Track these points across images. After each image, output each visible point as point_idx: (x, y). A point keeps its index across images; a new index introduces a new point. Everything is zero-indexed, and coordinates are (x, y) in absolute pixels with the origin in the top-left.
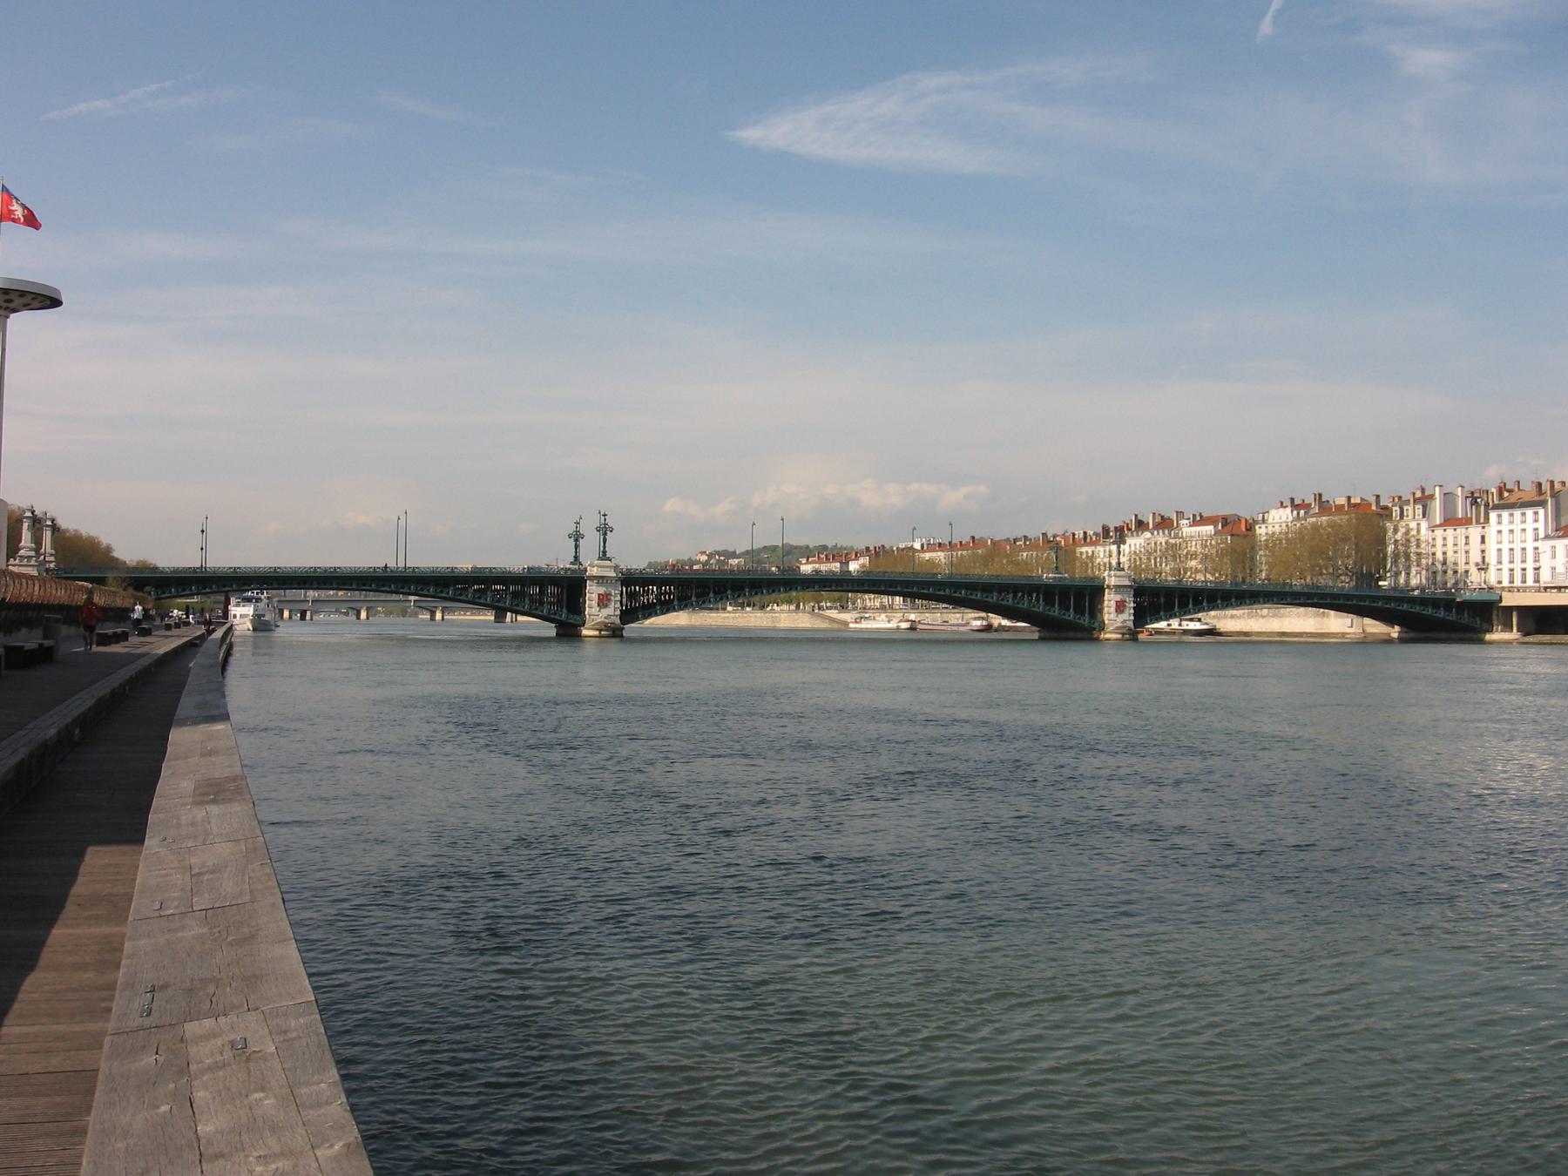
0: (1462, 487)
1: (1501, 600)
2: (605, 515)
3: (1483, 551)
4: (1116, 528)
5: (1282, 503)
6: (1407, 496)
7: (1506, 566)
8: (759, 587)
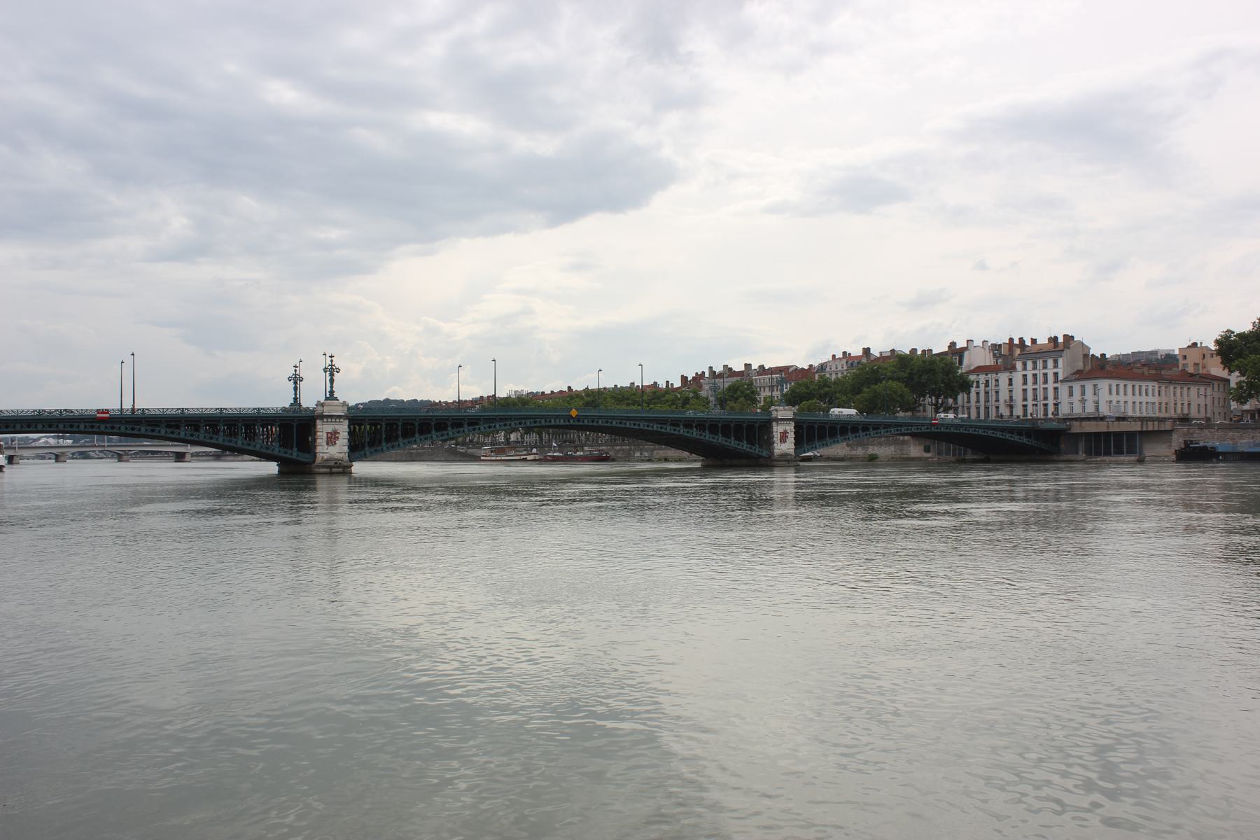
1: (1070, 429)
2: (331, 357)
3: (1011, 391)
4: (316, 405)
6: (322, 400)
7: (1041, 403)
8: (476, 424)
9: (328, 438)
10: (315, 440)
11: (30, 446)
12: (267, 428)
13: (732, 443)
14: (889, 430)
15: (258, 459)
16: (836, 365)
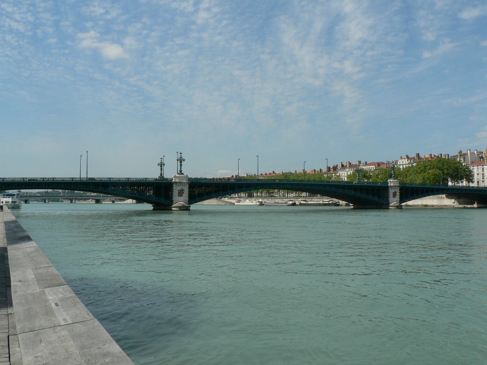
0: (477, 150)
2: (181, 153)
5: (401, 157)
9: (179, 193)
10: (172, 194)
11: (60, 195)
12: (141, 188)
13: (371, 197)
14: (444, 192)
15: (484, 206)
16: (403, 162)
